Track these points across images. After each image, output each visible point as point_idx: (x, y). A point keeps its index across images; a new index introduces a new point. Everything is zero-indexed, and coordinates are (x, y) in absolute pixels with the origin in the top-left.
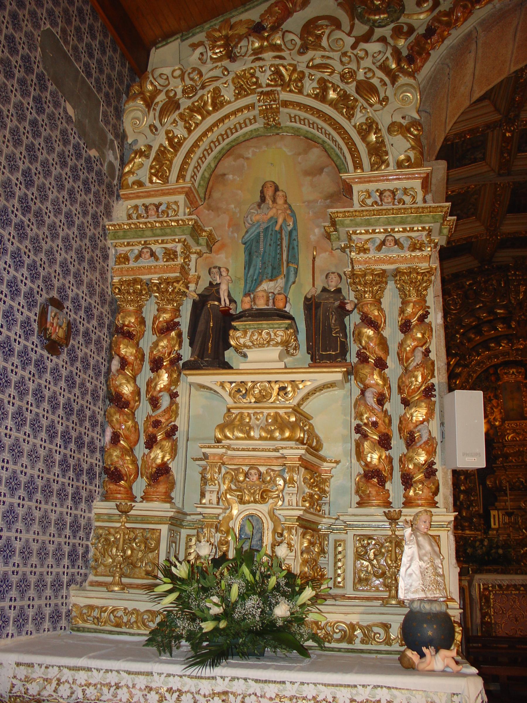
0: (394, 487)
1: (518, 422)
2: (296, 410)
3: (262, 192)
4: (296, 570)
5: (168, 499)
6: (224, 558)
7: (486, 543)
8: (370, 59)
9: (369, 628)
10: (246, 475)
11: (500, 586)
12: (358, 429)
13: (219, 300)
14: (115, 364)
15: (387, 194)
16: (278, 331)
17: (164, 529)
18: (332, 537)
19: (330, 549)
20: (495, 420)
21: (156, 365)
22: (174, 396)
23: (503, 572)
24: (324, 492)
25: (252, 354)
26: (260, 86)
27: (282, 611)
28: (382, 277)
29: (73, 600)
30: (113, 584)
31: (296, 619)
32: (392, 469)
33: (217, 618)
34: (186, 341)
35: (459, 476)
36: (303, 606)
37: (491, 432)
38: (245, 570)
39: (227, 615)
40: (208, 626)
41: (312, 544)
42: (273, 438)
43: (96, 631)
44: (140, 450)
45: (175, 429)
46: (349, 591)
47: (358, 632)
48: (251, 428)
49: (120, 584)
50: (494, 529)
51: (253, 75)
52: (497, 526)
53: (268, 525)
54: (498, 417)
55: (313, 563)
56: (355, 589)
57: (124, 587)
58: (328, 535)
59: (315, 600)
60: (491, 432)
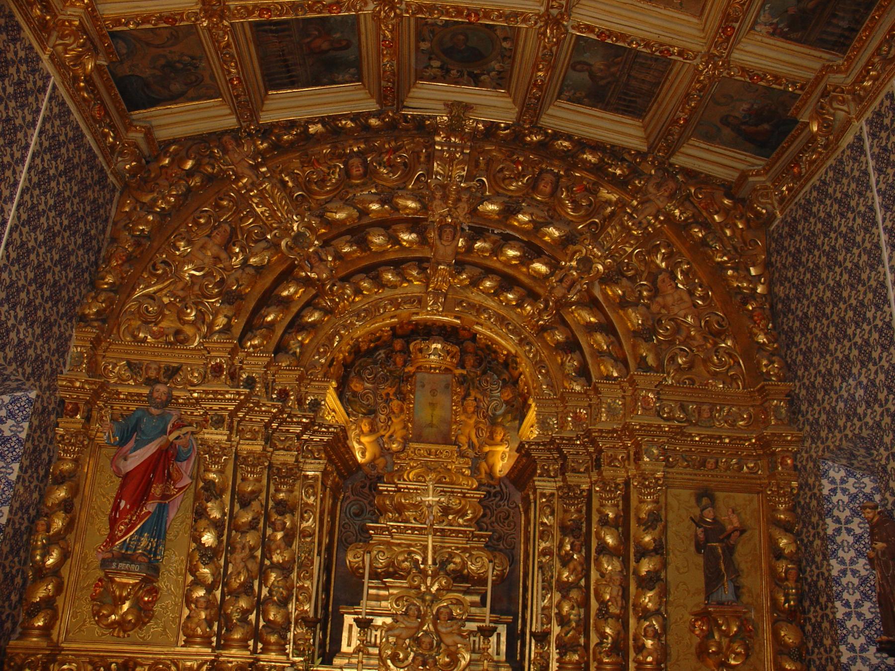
37: (381, 462)
54: (398, 435)
60: (381, 462)
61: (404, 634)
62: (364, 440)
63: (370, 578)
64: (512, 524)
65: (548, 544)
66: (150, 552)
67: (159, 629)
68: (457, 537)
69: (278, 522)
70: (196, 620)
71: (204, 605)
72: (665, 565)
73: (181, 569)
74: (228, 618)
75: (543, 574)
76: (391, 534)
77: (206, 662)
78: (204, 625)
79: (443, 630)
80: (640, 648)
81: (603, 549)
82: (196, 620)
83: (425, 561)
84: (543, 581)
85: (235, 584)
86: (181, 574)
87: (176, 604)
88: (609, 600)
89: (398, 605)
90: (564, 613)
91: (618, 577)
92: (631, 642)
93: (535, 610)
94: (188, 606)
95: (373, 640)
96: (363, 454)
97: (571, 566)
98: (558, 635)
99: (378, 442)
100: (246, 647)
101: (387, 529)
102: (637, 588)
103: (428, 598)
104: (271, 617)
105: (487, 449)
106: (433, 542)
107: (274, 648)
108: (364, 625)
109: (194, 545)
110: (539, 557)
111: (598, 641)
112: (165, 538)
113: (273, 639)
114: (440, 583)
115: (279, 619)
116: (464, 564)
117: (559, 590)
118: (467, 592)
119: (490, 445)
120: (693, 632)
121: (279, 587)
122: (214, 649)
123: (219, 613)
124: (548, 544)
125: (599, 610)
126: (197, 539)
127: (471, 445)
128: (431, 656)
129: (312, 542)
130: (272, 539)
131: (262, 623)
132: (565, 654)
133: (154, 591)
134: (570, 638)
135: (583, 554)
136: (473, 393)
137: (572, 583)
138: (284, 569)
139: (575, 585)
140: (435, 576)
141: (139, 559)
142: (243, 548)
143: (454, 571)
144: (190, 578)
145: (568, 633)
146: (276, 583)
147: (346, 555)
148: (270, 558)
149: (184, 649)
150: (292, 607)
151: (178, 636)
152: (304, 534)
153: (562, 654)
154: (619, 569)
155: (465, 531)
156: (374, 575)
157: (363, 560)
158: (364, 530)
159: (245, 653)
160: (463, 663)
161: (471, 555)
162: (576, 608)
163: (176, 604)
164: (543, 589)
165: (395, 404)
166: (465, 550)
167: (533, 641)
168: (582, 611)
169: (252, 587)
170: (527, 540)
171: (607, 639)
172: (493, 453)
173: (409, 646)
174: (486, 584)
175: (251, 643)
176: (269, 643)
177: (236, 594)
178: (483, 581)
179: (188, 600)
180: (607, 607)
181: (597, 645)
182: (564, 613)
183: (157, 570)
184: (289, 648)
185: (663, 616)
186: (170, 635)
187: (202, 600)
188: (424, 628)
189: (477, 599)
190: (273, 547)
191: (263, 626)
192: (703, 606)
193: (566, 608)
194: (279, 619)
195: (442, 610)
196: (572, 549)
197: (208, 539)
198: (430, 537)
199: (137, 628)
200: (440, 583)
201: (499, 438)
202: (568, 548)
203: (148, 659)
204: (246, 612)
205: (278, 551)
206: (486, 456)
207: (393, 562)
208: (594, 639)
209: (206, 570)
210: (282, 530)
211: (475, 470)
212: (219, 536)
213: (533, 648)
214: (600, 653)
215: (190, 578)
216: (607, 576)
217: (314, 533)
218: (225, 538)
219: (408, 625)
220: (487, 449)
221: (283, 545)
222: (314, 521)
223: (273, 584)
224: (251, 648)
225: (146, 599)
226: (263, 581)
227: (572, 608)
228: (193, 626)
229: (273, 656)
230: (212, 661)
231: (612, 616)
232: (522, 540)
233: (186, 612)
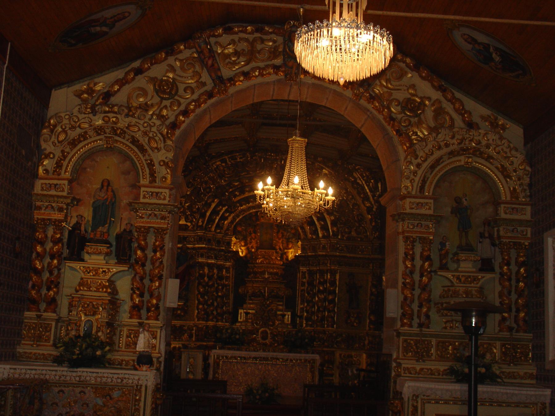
0: (144, 312)
1: (267, 251)
2: (109, 281)
3: (102, 183)
4: (104, 341)
5: (54, 312)
6: (79, 336)
7: (229, 331)
8: (155, 128)
9: (128, 361)
10: (88, 305)
11: (226, 357)
12: (132, 289)
13: (81, 231)
14: (34, 255)
15: (155, 194)
16: (103, 248)
17: (54, 324)
18: (119, 329)
19: (118, 333)
20: (252, 247)
21: (52, 257)
22: (59, 270)
23: (238, 350)
24: (117, 312)
25: (94, 257)
26: (106, 134)
27: (99, 353)
28: (147, 230)
29: (18, 350)
30: (34, 344)
31: (103, 356)
32: (143, 305)
33: (78, 354)
34: (65, 247)
35: (169, 309)
36: (106, 352)
37: (249, 255)
38: (88, 339)
39: (81, 353)
40: (75, 357)
41: (110, 331)
42: (99, 291)
43: (27, 361)
44: (44, 291)
45: (59, 283)
46: (123, 349)
47: (124, 362)
48: (91, 287)
49: (36, 344)
50: (240, 322)
51: (103, 129)
52: (242, 320)
53: (95, 324)
54: (255, 246)
55: (111, 338)
56: (125, 348)
57: (38, 346)
58: (117, 328)
59: (109, 351)
60: (249, 255)
62: (242, 248)
96: (242, 253)
99: (248, 249)
105: (286, 251)
113: (220, 318)
118: (279, 301)
119: (287, 249)
127: (280, 249)
136: (281, 231)
165: (253, 235)
172: (288, 252)
201: (290, 246)
204: (212, 311)
206: (285, 253)
211: (282, 257)
220: (286, 251)
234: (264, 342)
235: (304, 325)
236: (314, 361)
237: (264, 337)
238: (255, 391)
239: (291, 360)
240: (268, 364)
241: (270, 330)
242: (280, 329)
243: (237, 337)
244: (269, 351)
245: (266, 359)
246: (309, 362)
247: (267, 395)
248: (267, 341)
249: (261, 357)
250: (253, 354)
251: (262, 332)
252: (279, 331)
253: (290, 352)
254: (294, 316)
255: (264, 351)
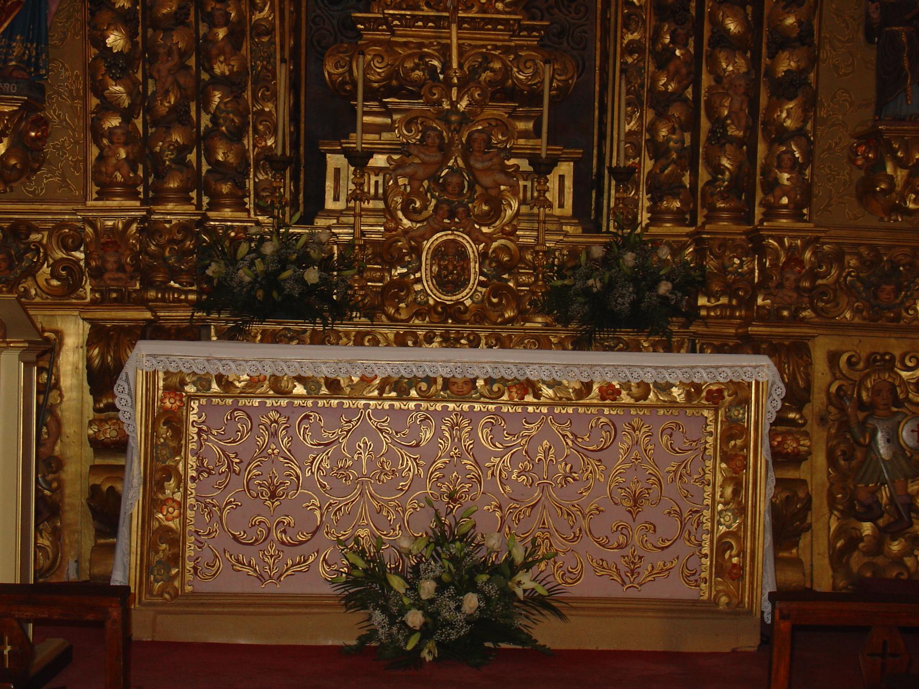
11: (333, 385)
52: (341, 205)
61: (421, 172)
63: (365, 99)
64: (583, 9)
65: (636, 36)
66: (28, 63)
67: (56, 179)
68: (495, 29)
69: (217, 13)
70: (113, 161)
71: (122, 139)
72: (814, 61)
73: (78, 90)
74: (157, 159)
75: (628, 82)
76: (391, 29)
77: (133, 220)
78: (126, 168)
79: (479, 165)
80: (771, 185)
81: (721, 39)
82: (113, 161)
83: (446, 66)
84: (628, 92)
85: (163, 107)
86: (78, 97)
87: (77, 143)
88: (727, 117)
89: (409, 131)
90: (661, 139)
91: (742, 82)
92: (758, 178)
93: (615, 136)
94: (97, 142)
95: (372, 191)
97: (671, 67)
98: (650, 173)
100: (188, 200)
101: (385, 20)
102: (770, 98)
103: (453, 118)
104: (220, 158)
106: (459, 38)
107: (227, 201)
108: (359, 160)
109: (94, 51)
110: (622, 56)
111: (710, 178)
112: (47, 44)
113: (225, 189)
114: (472, 96)
115: (231, 159)
116: (506, 72)
117: (651, 106)
120: (854, 162)
121: (228, 113)
122: (144, 202)
123: (143, 152)
124: (636, 36)
125: (712, 131)
126: (99, 42)
128: (461, 204)
129: (272, 43)
130: (209, 39)
131: (205, 168)
132: (661, 200)
133: (42, 123)
134: (668, 175)
135: (692, 50)
137: (672, 93)
138: (233, 85)
139: (678, 96)
140: (463, 87)
141: (15, 74)
142: (170, 53)
143: (490, 83)
144: (94, 102)
145: (666, 169)
146: (222, 107)
147: (322, 65)
148: (210, 70)
149: (100, 203)
150: (248, 142)
151: (85, 187)
152: (259, 30)
153: (656, 200)
154: (744, 69)
155: (508, 20)
156: (371, 94)
157: (350, 71)
158: (349, 26)
159: (187, 207)
160: (509, 213)
161: (517, 57)
162: (678, 131)
163: (77, 143)
164: (628, 104)
166: (507, 50)
167: (613, 183)
168: (687, 137)
169: (188, 112)
170: (605, 31)
171: (723, 174)
173: (428, 190)
174: (540, 103)
175: (193, 194)
176: (221, 195)
177: (163, 124)
178: (534, 97)
179: (97, 134)
180: (725, 127)
181: (708, 183)
182: (661, 139)
183: (42, 90)
184: (250, 202)
185: (808, 139)
186: (73, 186)
187: (119, 131)
188: (450, 164)
189: (530, 125)
190: (214, 51)
191: (208, 171)
192: (870, 124)
193: (664, 132)
194: (231, 159)
195: (476, 135)
196: (672, 41)
197: (115, 40)
198: (454, 27)
199: (23, 179)
200: (472, 96)
202: (667, 40)
203: (46, 221)
205: (222, 58)
207: (398, 72)
208: (704, 176)
209: (118, 88)
210: (225, 25)
212: (131, 36)
213: (613, 192)
214: (712, 195)
215: (94, 102)
216: (725, 81)
217: (274, 29)
218: (139, 39)
219: (427, 159)
221: (228, 49)
222: (272, 9)
223: (218, 106)
224: (194, 201)
225: (33, 134)
226: (204, 103)
227: (672, 131)
228: (110, 170)
229: (227, 213)
230: (143, 219)
231: (733, 140)
232: (599, 34)
233: (95, 151)
234: (449, 299)
235: (644, 217)
236: (740, 392)
237: (450, 281)
238: (397, 583)
239: (609, 393)
240: (473, 417)
241: (477, 241)
242: (526, 236)
243: (312, 275)
244: (474, 343)
245: (458, 388)
246: (715, 397)
247: (471, 602)
248: (464, 298)
249: (430, 381)
250: (388, 360)
251: (438, 254)
252: (523, 248)
253: (581, 343)
254: (587, 186)
255: (450, 341)
